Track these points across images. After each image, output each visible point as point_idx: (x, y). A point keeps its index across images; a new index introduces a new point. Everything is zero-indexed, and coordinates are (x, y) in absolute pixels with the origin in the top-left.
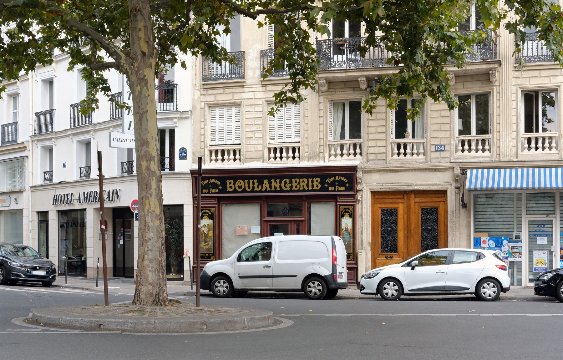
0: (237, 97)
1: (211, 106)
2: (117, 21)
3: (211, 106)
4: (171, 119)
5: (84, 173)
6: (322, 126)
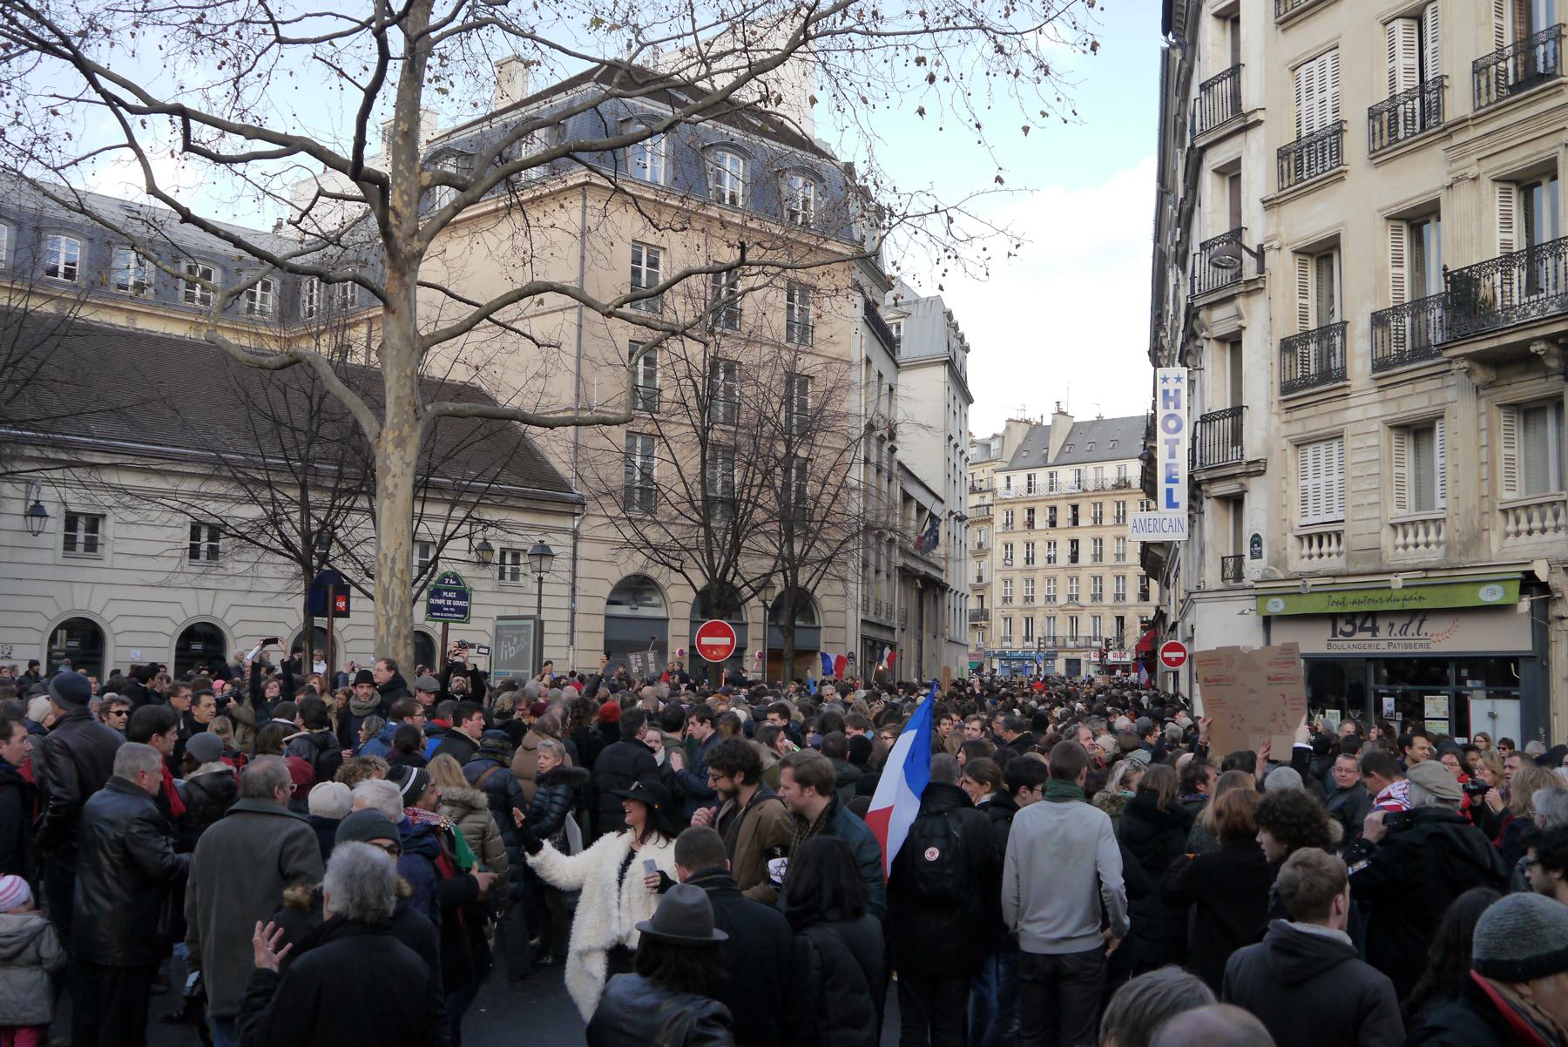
0: (1337, 419)
1: (1300, 444)
2: (279, 510)
3: (1300, 444)
4: (1233, 476)
5: (1229, 573)
6: (1484, 468)
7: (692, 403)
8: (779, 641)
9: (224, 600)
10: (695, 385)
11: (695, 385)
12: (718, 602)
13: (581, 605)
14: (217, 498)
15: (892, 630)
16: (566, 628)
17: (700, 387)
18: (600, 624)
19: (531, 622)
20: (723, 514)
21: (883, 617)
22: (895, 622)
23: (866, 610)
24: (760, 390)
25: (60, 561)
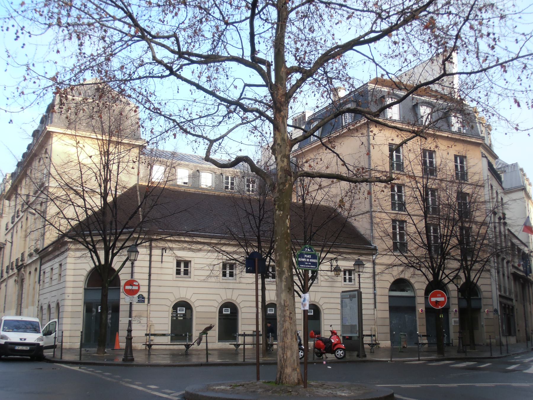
7: (419, 198)
8: (464, 304)
9: (236, 293)
10: (420, 191)
11: (420, 191)
12: (435, 285)
13: (378, 291)
14: (225, 244)
15: (511, 300)
16: (372, 301)
17: (422, 192)
18: (387, 299)
19: (356, 293)
20: (436, 249)
21: (508, 294)
22: (513, 296)
23: (500, 291)
24: (448, 196)
25: (175, 279)
